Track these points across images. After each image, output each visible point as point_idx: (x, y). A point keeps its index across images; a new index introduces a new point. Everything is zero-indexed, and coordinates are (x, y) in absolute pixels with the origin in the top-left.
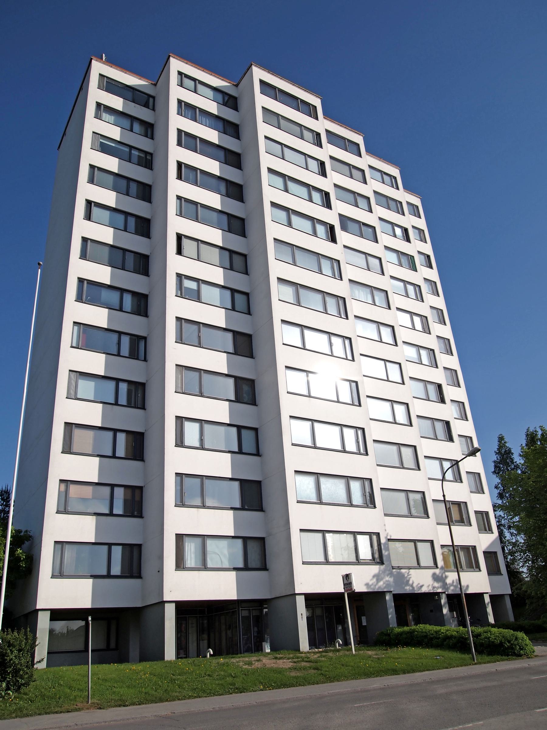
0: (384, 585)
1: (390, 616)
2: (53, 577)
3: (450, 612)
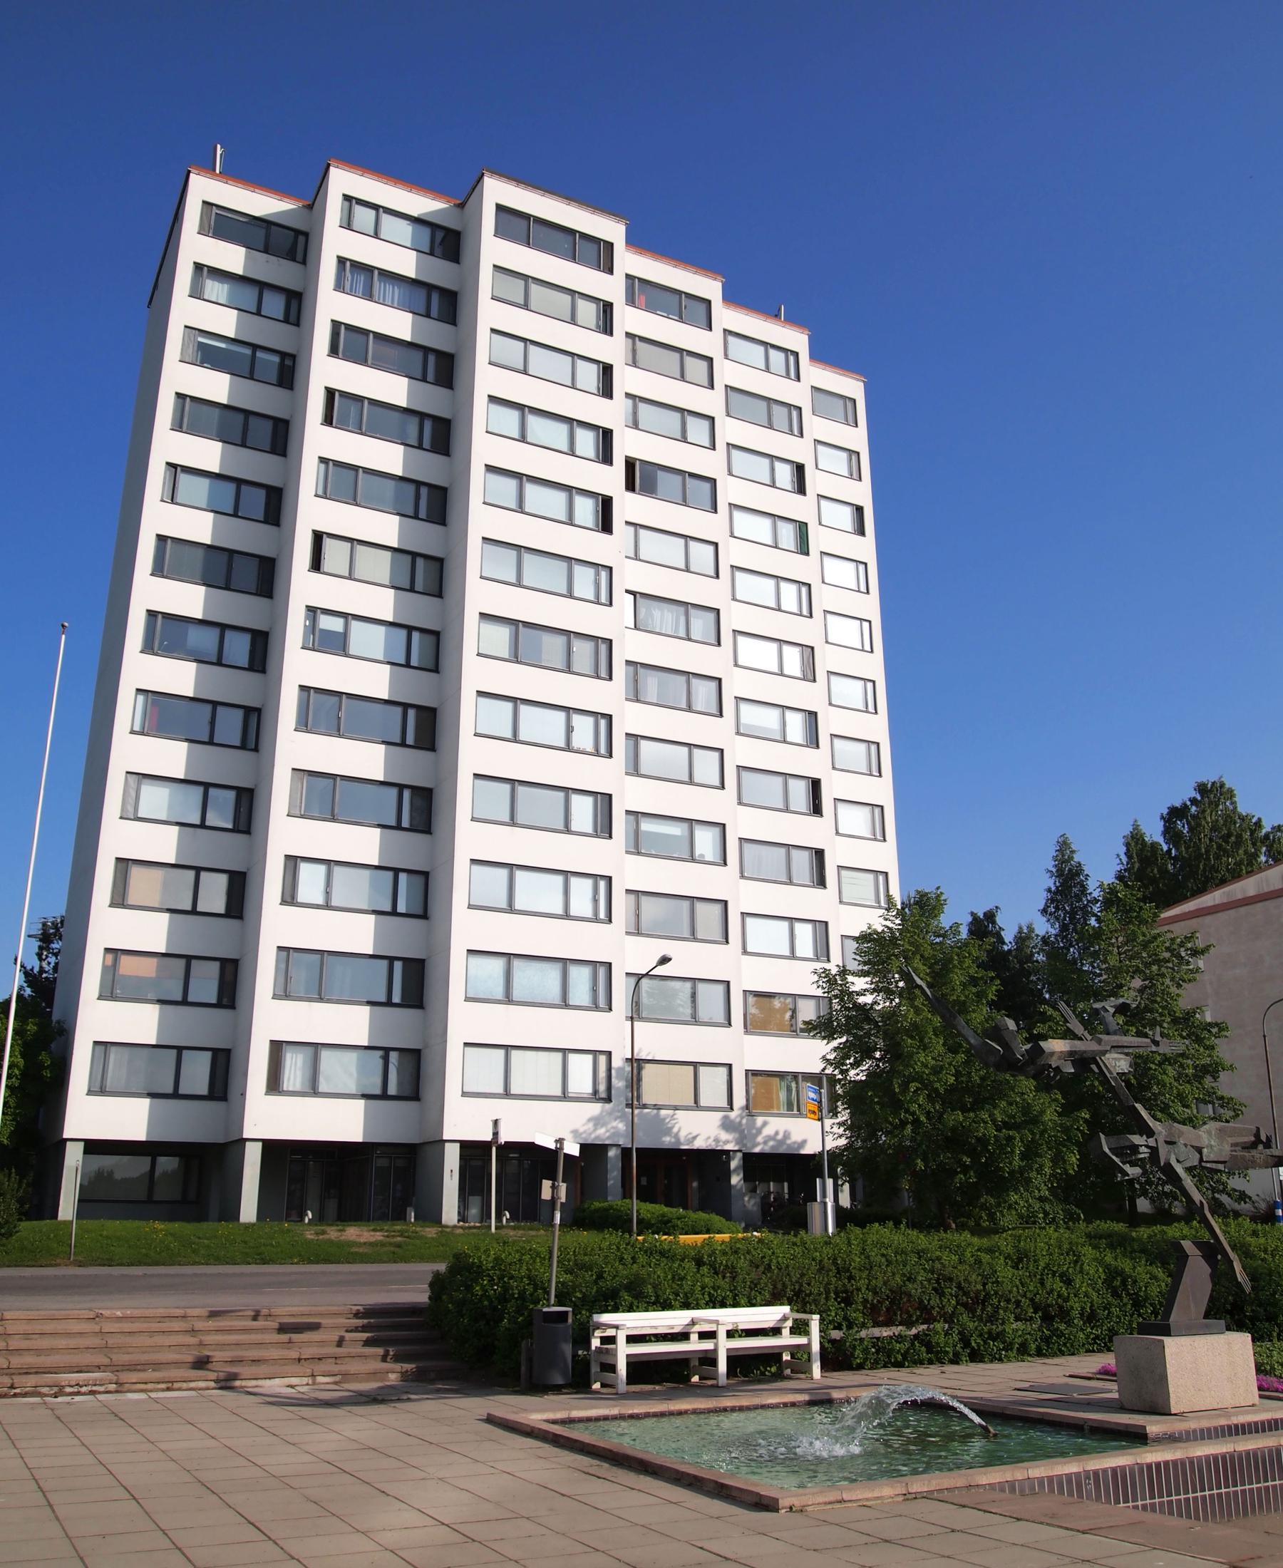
0: (608, 1134)
1: (610, 1183)
2: (90, 1093)
3: (744, 1181)
